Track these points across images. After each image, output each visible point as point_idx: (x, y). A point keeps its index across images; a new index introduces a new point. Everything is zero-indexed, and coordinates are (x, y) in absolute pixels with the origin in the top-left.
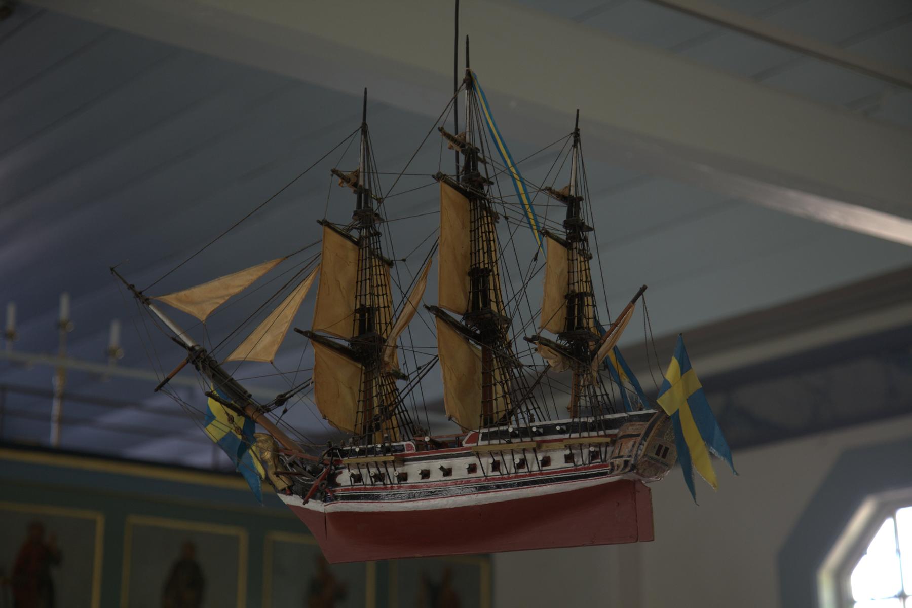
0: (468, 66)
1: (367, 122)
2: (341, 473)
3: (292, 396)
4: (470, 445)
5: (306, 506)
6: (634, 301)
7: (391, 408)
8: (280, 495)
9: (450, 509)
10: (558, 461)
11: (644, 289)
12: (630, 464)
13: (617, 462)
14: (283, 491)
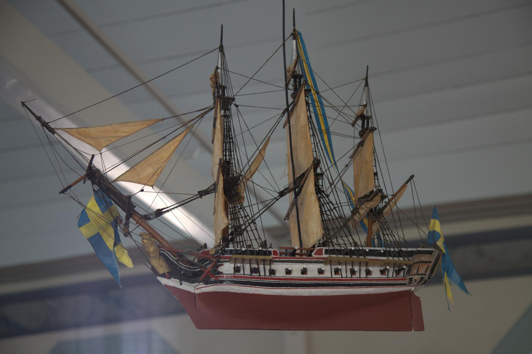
0: (294, 25)
1: (223, 44)
2: (222, 265)
3: (168, 211)
4: (317, 256)
5: (181, 287)
6: (407, 182)
7: (243, 227)
8: (159, 278)
9: (306, 296)
10: (376, 273)
11: (412, 177)
12: (424, 280)
13: (416, 277)
14: (163, 276)
